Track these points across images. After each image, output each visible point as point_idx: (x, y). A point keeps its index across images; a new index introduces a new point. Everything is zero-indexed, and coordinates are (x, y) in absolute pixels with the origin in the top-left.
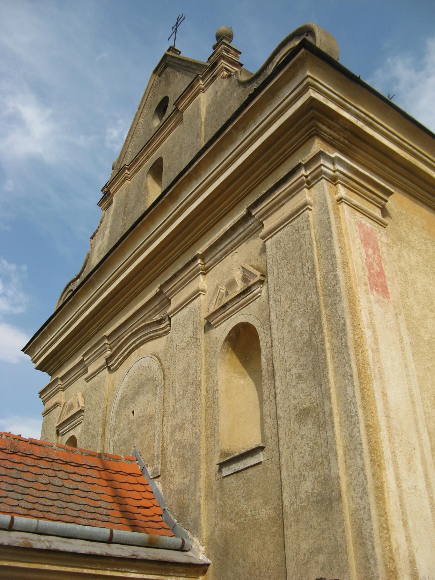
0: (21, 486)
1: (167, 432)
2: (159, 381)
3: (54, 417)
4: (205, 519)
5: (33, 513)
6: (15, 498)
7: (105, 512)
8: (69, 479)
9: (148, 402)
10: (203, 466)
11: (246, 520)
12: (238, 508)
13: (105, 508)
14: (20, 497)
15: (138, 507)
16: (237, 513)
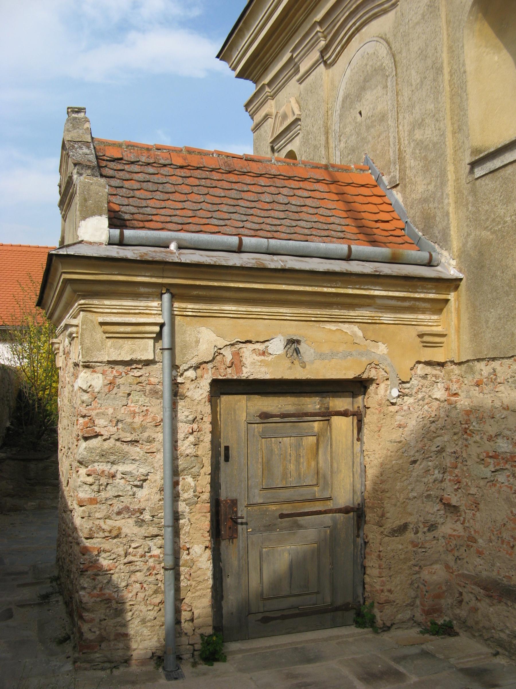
0: (243, 207)
1: (404, 131)
2: (390, 70)
3: (266, 132)
4: (456, 229)
5: (260, 233)
6: (239, 219)
7: (339, 228)
8: (294, 195)
9: (377, 98)
10: (450, 168)
11: (504, 227)
12: (494, 214)
13: (338, 224)
14: (244, 218)
15: (376, 221)
16: (494, 220)
